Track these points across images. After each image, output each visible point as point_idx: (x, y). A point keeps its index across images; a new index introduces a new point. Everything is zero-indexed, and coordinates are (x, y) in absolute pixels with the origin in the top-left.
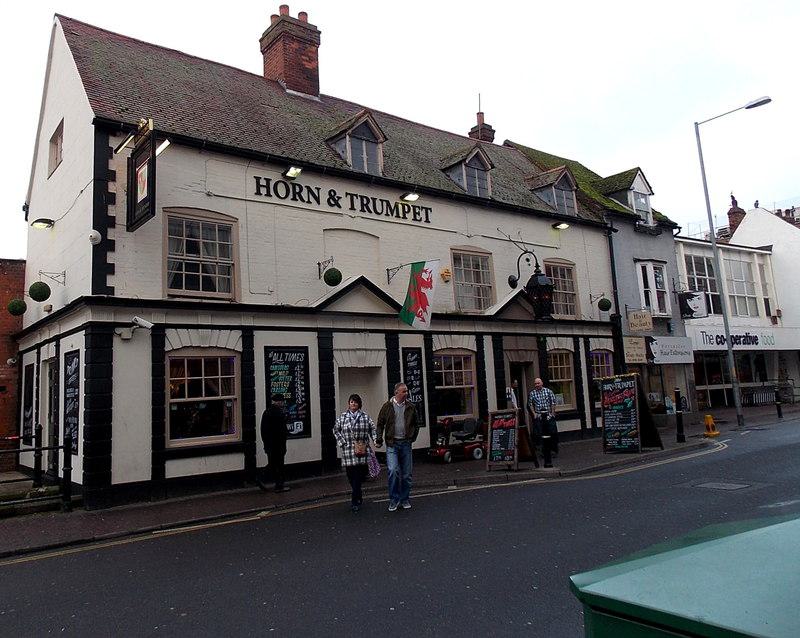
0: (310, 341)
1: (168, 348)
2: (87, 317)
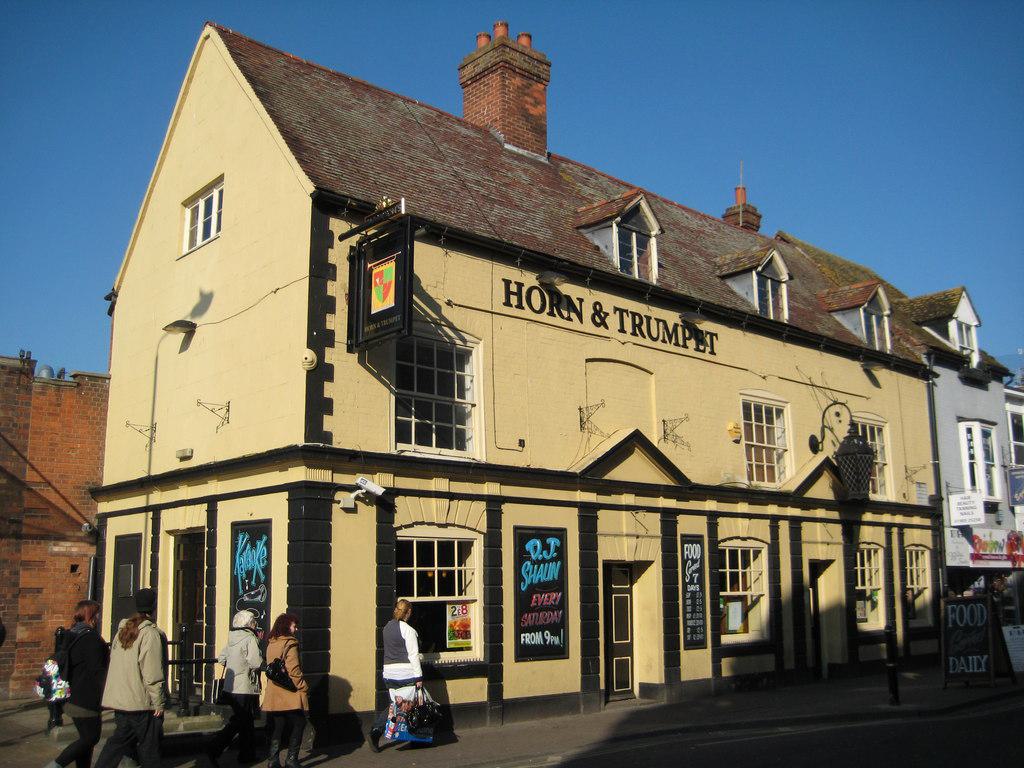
0: (568, 520)
2: (298, 474)
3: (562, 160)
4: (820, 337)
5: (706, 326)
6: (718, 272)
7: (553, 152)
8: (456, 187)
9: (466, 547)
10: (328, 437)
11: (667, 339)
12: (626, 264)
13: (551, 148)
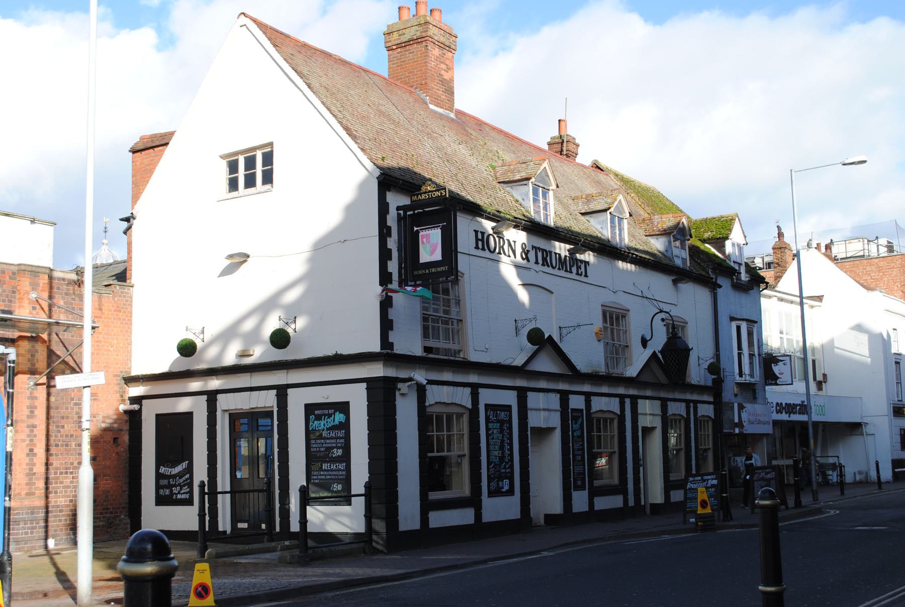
0: (509, 398)
1: (427, 404)
13: (458, 105)
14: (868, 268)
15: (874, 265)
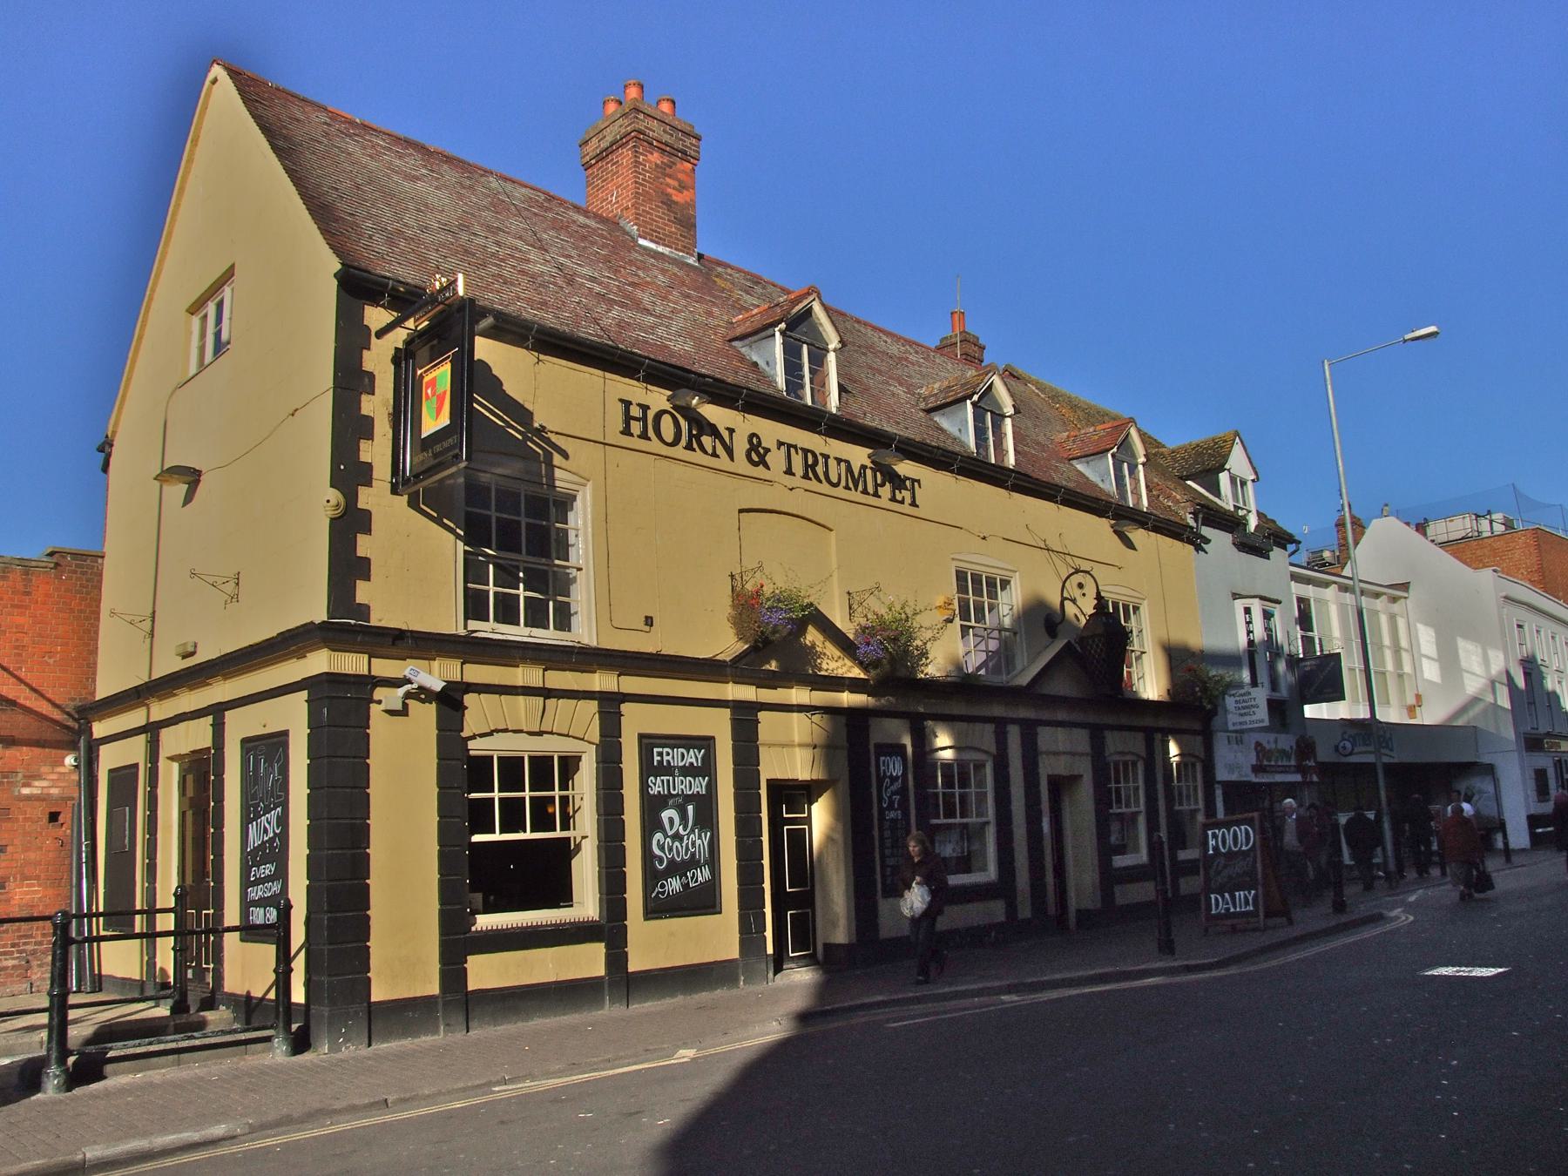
0: (718, 725)
2: (319, 662)
3: (719, 264)
4: (1057, 488)
5: (905, 468)
6: (923, 405)
7: (707, 253)
8: (560, 282)
9: (570, 765)
10: (364, 611)
11: (851, 485)
12: (794, 382)
14: (1479, 553)
15: (1486, 547)
